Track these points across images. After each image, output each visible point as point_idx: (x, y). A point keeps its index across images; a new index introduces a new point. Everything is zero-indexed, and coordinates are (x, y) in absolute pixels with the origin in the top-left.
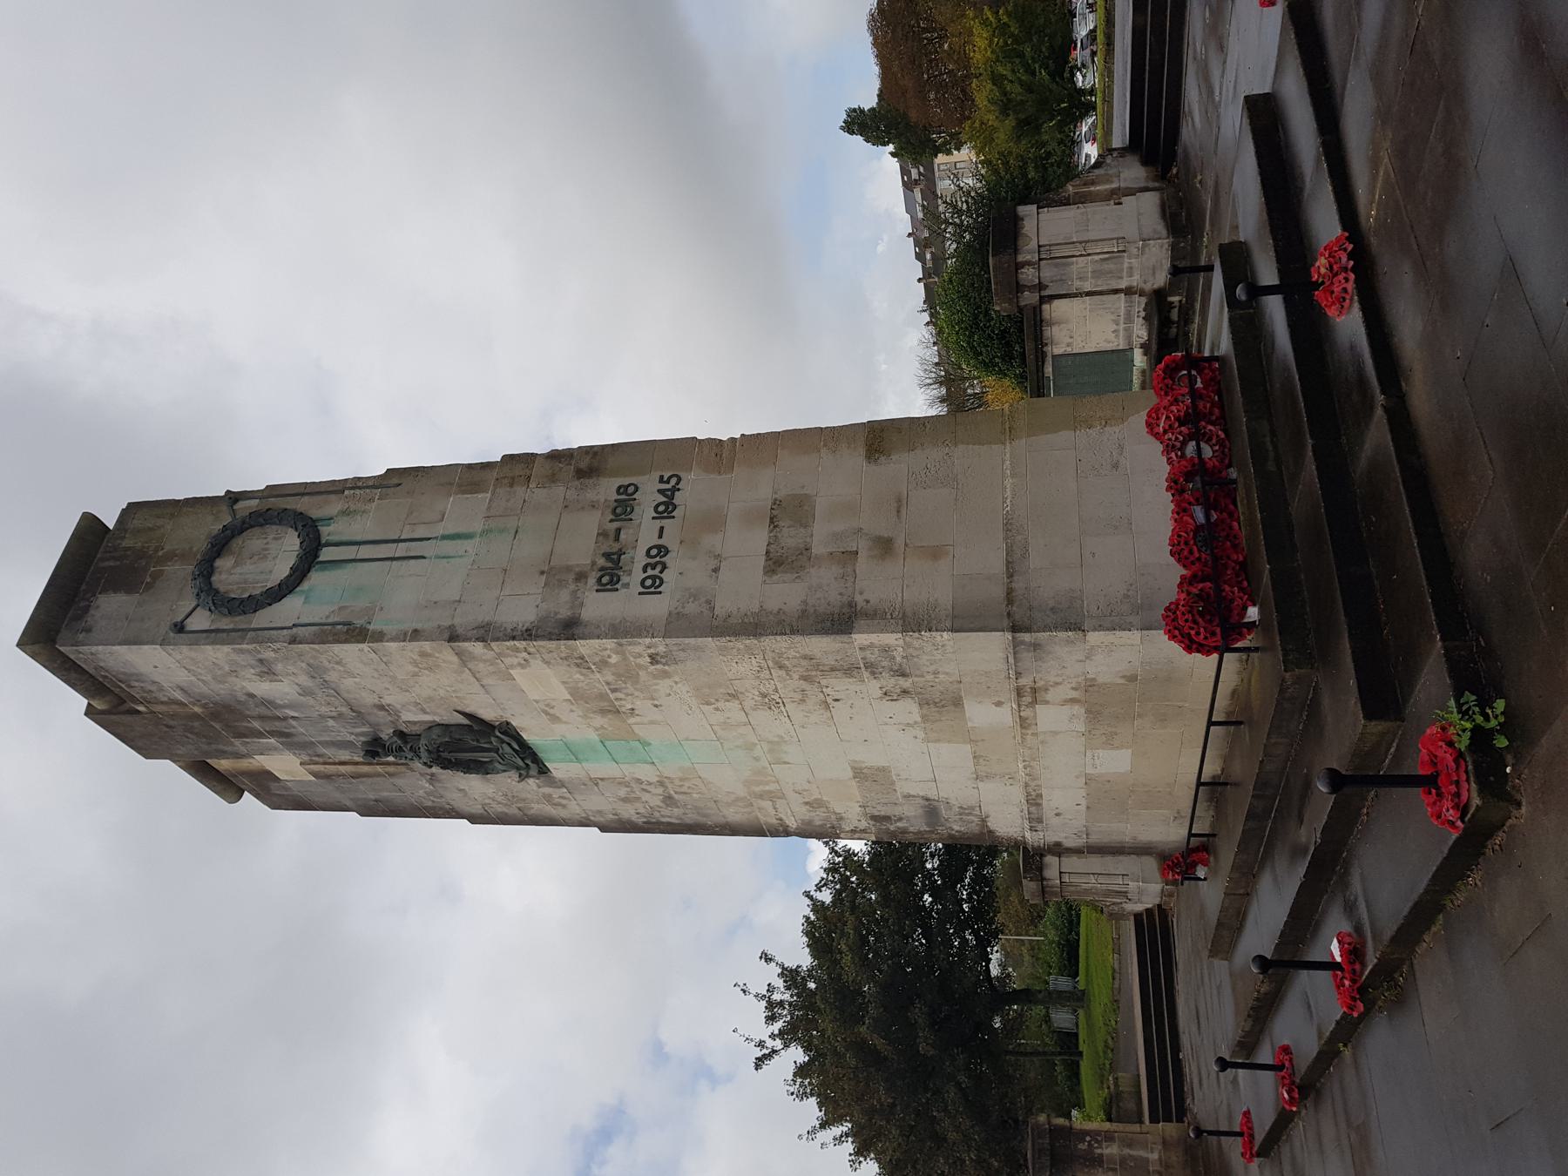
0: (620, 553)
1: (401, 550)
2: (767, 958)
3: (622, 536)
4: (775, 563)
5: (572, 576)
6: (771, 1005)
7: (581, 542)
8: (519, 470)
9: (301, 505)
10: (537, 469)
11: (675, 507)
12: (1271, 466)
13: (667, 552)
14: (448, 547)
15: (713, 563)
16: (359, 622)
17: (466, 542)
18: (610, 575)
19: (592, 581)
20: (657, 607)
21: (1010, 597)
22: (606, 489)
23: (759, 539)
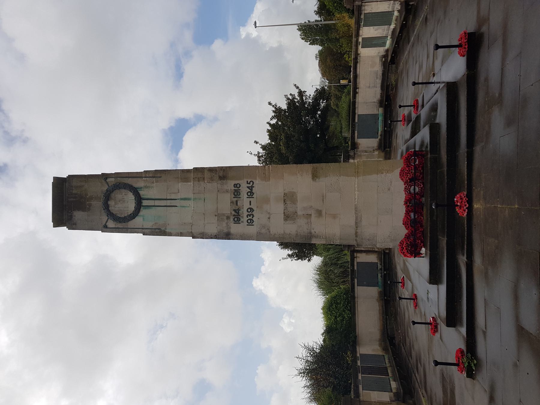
0: (239, 210)
1: (168, 203)
2: (256, 142)
3: (238, 204)
4: (287, 217)
5: (225, 218)
6: (259, 157)
7: (225, 204)
8: (200, 175)
9: (129, 181)
10: (207, 175)
11: (253, 194)
12: (435, 218)
13: (253, 210)
14: (184, 203)
15: (268, 216)
16: (163, 229)
17: (189, 201)
18: (237, 219)
19: (232, 219)
20: (253, 230)
21: (356, 233)
22: (230, 185)
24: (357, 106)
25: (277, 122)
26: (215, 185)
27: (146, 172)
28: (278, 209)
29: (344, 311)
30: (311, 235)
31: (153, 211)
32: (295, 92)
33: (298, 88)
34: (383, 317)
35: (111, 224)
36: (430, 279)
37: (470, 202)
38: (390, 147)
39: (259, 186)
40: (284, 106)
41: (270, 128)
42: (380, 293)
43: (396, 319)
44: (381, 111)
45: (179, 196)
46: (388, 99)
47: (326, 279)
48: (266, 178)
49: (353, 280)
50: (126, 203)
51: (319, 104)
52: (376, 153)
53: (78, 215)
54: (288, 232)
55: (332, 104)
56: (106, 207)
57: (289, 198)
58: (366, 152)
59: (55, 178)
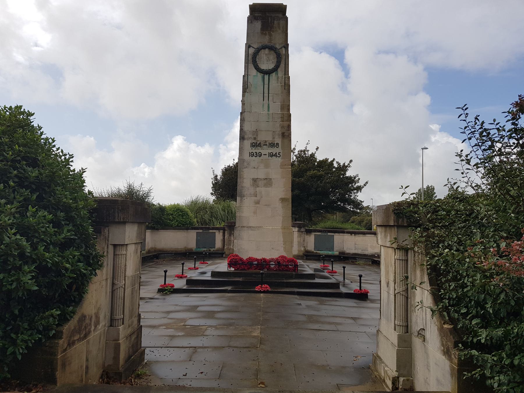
0: (260, 146)
1: (266, 95)
2: (317, 149)
5: (255, 136)
6: (304, 151)
8: (286, 118)
9: (282, 65)
12: (254, 275)
16: (247, 90)
19: (254, 141)
21: (244, 227)
22: (278, 140)
23: (262, 176)
24: (341, 234)
25: (334, 167)
26: (278, 130)
27: (289, 78)
28: (261, 174)
29: (177, 221)
30: (242, 196)
31: (261, 83)
32: (361, 183)
33: (365, 185)
34: (173, 251)
35: (252, 51)
36: (214, 272)
37: (264, 292)
38: (306, 259)
39: (276, 161)
40: (348, 174)
41: (329, 161)
42: (191, 249)
43: (171, 260)
44: (336, 253)
45: (271, 103)
46: (345, 258)
47: (198, 207)
48: (282, 166)
49: (201, 229)
50: (267, 62)
51: (349, 205)
52: (303, 249)
53: (258, 25)
54: (245, 181)
55: (355, 217)
56: (264, 47)
57: (268, 182)
58: (304, 241)
59: (285, 7)
